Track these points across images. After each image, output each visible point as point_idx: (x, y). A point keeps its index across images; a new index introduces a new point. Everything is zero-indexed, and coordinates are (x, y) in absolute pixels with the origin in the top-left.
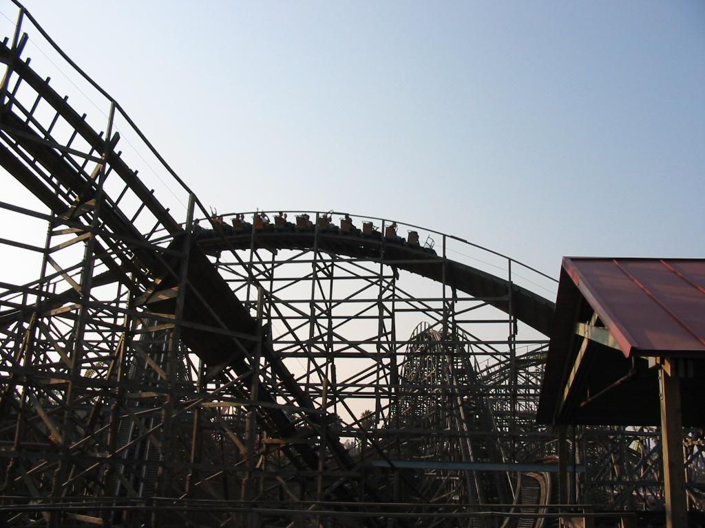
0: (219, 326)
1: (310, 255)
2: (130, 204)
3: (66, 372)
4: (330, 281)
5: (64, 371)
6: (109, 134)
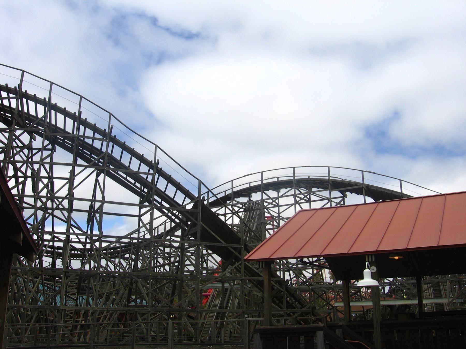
0: (220, 242)
1: (292, 192)
2: (171, 191)
3: (392, 287)
4: (309, 203)
5: (393, 287)
6: (155, 161)
